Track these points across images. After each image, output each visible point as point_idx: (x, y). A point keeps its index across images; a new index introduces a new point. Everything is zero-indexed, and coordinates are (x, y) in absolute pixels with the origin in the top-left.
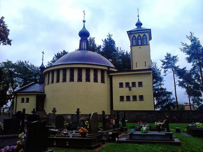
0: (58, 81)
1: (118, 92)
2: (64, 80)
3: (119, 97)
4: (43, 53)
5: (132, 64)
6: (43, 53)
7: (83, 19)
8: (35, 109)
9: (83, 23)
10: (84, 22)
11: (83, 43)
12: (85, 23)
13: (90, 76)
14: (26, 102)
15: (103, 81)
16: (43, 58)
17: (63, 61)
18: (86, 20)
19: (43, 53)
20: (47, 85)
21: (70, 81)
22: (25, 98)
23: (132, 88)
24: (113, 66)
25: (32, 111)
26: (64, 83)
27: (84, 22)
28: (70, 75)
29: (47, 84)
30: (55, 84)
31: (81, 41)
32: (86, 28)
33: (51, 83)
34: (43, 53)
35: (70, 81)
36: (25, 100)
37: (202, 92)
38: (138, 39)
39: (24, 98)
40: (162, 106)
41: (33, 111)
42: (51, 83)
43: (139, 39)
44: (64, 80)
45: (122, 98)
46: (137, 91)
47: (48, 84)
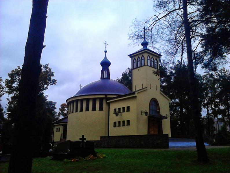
0: (81, 110)
1: (114, 118)
2: (87, 109)
3: (113, 123)
5: (166, 98)
7: (104, 50)
10: (106, 52)
11: (105, 72)
15: (101, 109)
18: (107, 50)
21: (92, 110)
23: (122, 113)
26: (87, 112)
27: (106, 52)
28: (93, 104)
29: (71, 112)
30: (79, 113)
31: (103, 71)
33: (75, 112)
35: (92, 110)
37: (14, 94)
38: (138, 61)
40: (216, 131)
42: (75, 112)
43: (139, 61)
44: (87, 109)
45: (115, 125)
46: (125, 116)
47: (73, 112)
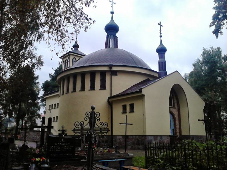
4: (161, 25)
6: (160, 24)
8: (53, 122)
9: (111, 15)
10: (112, 13)
11: (110, 40)
12: (113, 15)
13: (106, 81)
14: (130, 112)
16: (161, 33)
17: (79, 64)
19: (160, 24)
20: (53, 109)
22: (128, 104)
24: (96, 124)
25: (53, 128)
27: (112, 13)
32: (115, 22)
34: (161, 25)
36: (128, 109)
39: (126, 105)
41: (52, 129)
